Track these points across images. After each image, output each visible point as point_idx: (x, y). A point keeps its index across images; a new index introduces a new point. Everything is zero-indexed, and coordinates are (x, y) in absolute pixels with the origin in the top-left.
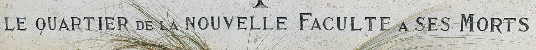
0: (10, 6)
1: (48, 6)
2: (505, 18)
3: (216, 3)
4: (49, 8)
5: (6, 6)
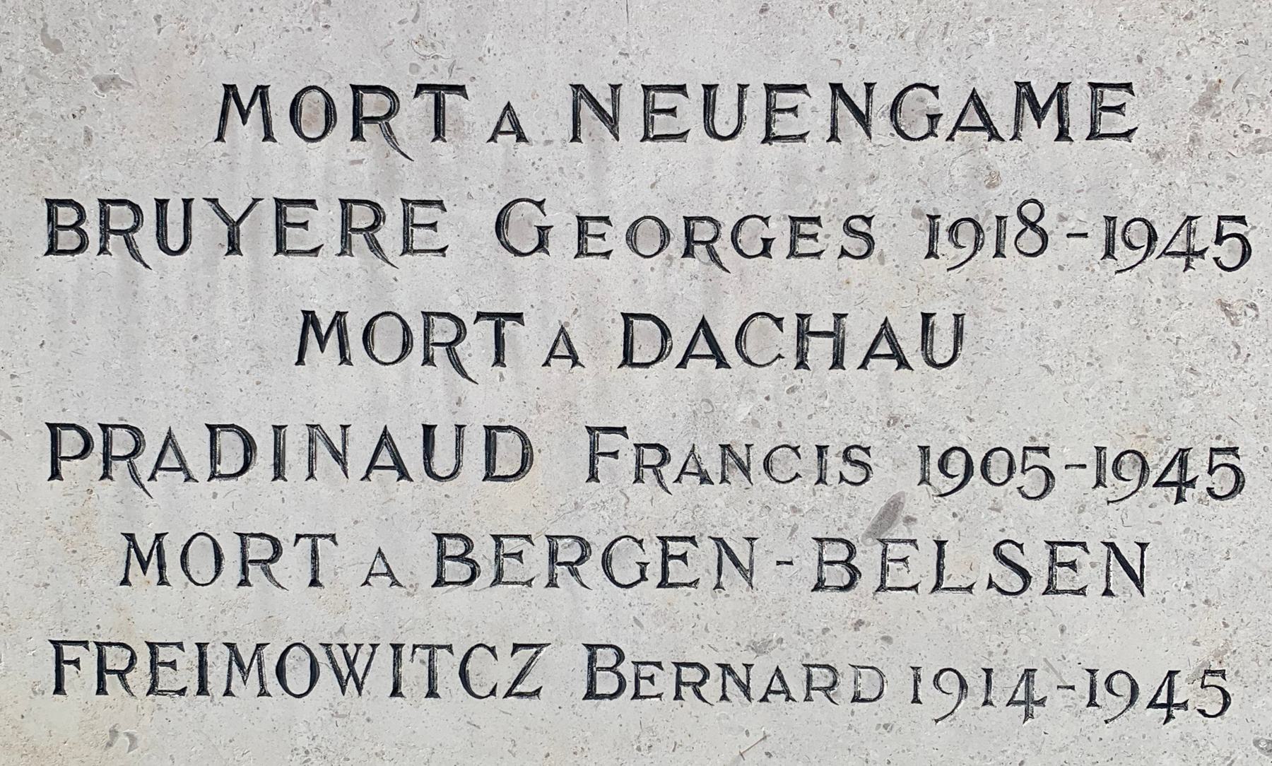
0: (127, 739)
1: (303, 742)
2: (483, 310)
3: (1095, 739)
4: (307, 752)
5: (108, 739)
